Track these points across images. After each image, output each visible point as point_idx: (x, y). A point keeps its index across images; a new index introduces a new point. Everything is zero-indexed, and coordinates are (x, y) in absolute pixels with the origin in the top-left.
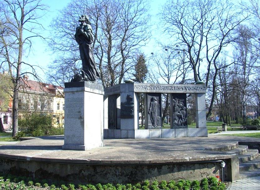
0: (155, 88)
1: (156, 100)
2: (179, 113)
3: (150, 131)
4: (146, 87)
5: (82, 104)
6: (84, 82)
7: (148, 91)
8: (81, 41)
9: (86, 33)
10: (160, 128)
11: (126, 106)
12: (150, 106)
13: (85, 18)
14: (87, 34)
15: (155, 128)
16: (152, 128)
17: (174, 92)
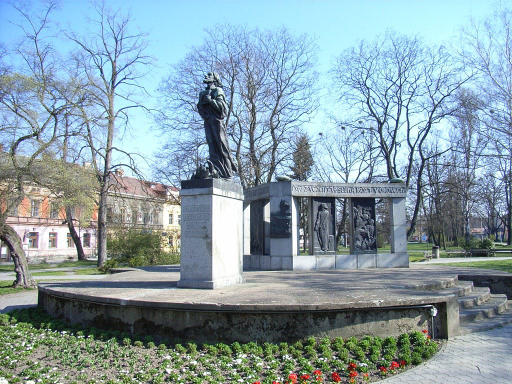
0: (326, 189)
2: (363, 230)
4: (310, 187)
5: (209, 214)
7: (315, 195)
9: (214, 101)
12: (317, 218)
13: (213, 77)
14: (217, 103)
15: (325, 254)
16: (321, 254)
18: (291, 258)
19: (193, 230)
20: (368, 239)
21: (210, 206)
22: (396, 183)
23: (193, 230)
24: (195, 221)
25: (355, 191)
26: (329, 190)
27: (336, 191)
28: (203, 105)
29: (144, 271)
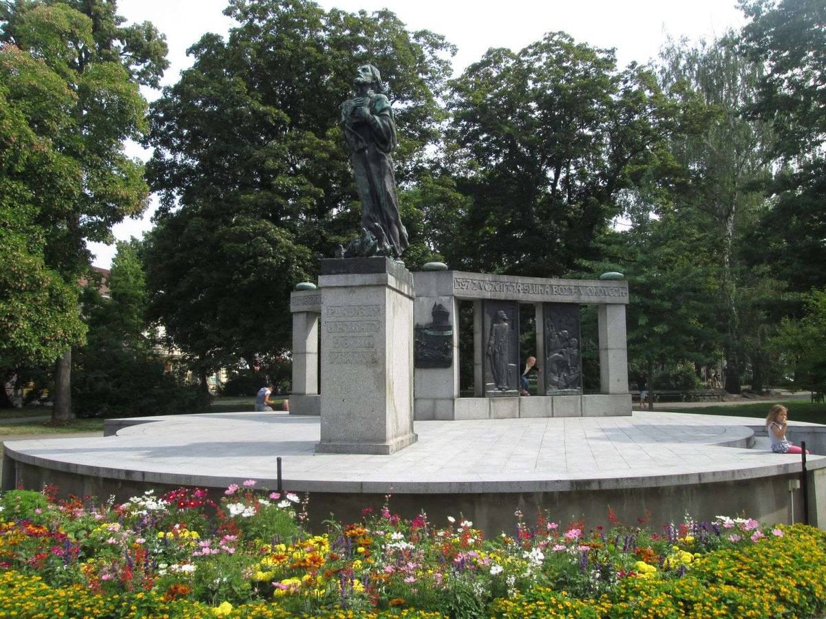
0: (505, 288)
1: (505, 320)
2: (561, 356)
3: (492, 404)
4: (482, 283)
5: (379, 322)
6: (384, 260)
7: (488, 295)
8: (362, 141)
9: (377, 118)
10: (515, 393)
11: (430, 333)
12: (491, 334)
13: (371, 74)
14: (381, 121)
15: (503, 395)
16: (495, 395)
17: (550, 301)
18: (451, 402)
19: (347, 350)
20: (568, 371)
21: (381, 307)
22: (611, 280)
23: (347, 350)
24: (351, 334)
25: (549, 293)
26: (510, 288)
27: (521, 291)
28: (354, 123)
29: (280, 424)
